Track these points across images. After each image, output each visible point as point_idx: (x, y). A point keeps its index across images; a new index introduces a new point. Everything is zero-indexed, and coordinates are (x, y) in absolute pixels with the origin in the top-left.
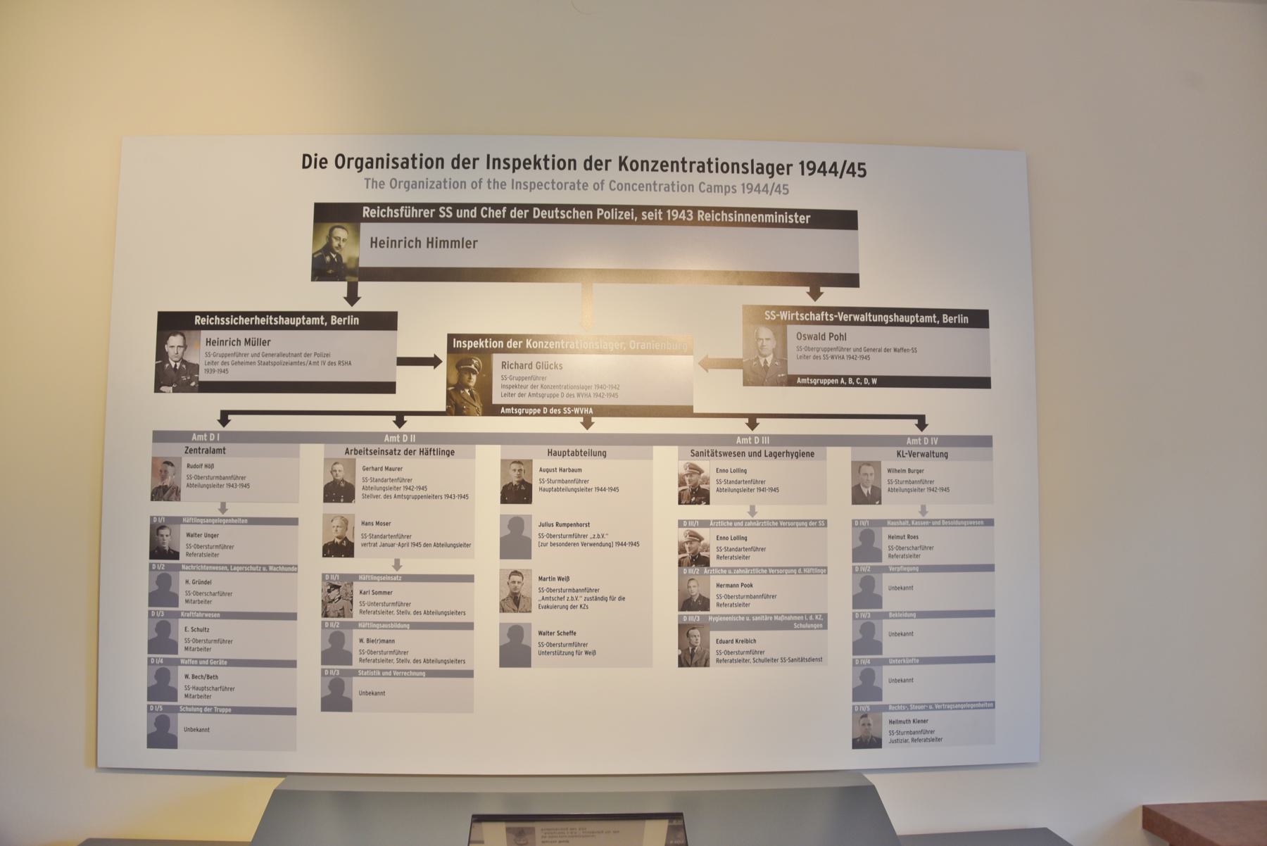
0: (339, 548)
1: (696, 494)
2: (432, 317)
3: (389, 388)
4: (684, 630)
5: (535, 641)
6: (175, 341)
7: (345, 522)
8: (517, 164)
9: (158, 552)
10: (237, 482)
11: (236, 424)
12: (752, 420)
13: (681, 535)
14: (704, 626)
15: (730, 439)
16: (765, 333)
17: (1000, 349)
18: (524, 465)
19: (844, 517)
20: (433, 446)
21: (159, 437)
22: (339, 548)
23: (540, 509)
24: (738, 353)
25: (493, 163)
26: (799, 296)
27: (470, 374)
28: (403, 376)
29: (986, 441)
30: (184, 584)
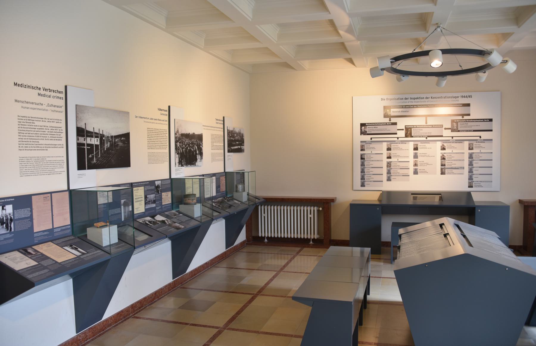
0: (389, 157)
1: (443, 149)
2: (402, 123)
3: (396, 134)
4: (442, 169)
5: (419, 171)
6: (363, 127)
7: (390, 154)
8: (415, 99)
9: (362, 158)
10: (373, 148)
11: (373, 140)
12: (452, 137)
13: (441, 155)
14: (445, 169)
15: (449, 140)
16: (455, 124)
17: (495, 125)
18: (417, 145)
19: (467, 152)
20: (403, 142)
21: (361, 142)
22: (389, 157)
23: (419, 151)
24: (450, 127)
25: (411, 98)
26: (460, 118)
27: (408, 132)
28: (398, 132)
29: (491, 140)
30: (366, 163)
